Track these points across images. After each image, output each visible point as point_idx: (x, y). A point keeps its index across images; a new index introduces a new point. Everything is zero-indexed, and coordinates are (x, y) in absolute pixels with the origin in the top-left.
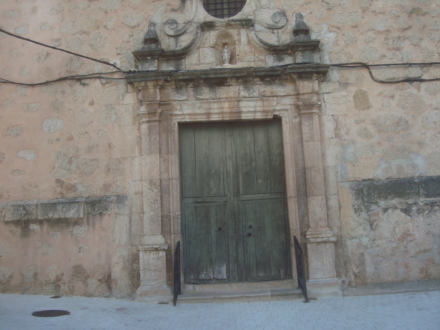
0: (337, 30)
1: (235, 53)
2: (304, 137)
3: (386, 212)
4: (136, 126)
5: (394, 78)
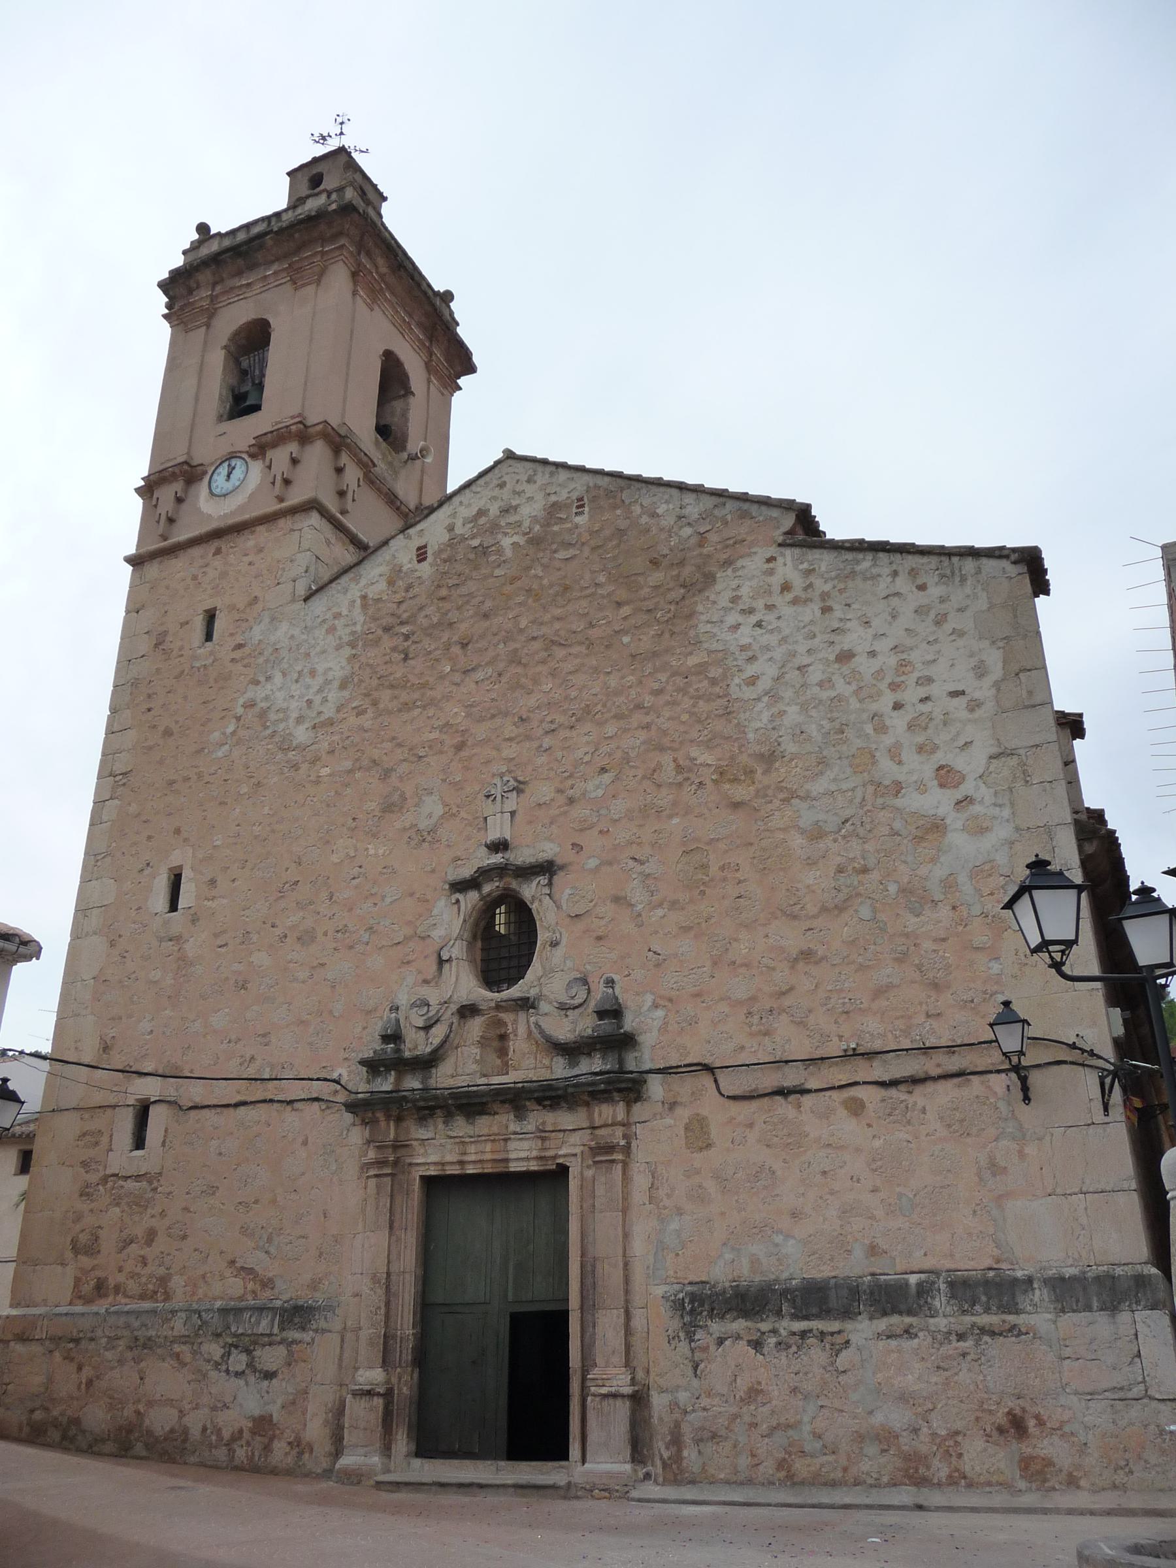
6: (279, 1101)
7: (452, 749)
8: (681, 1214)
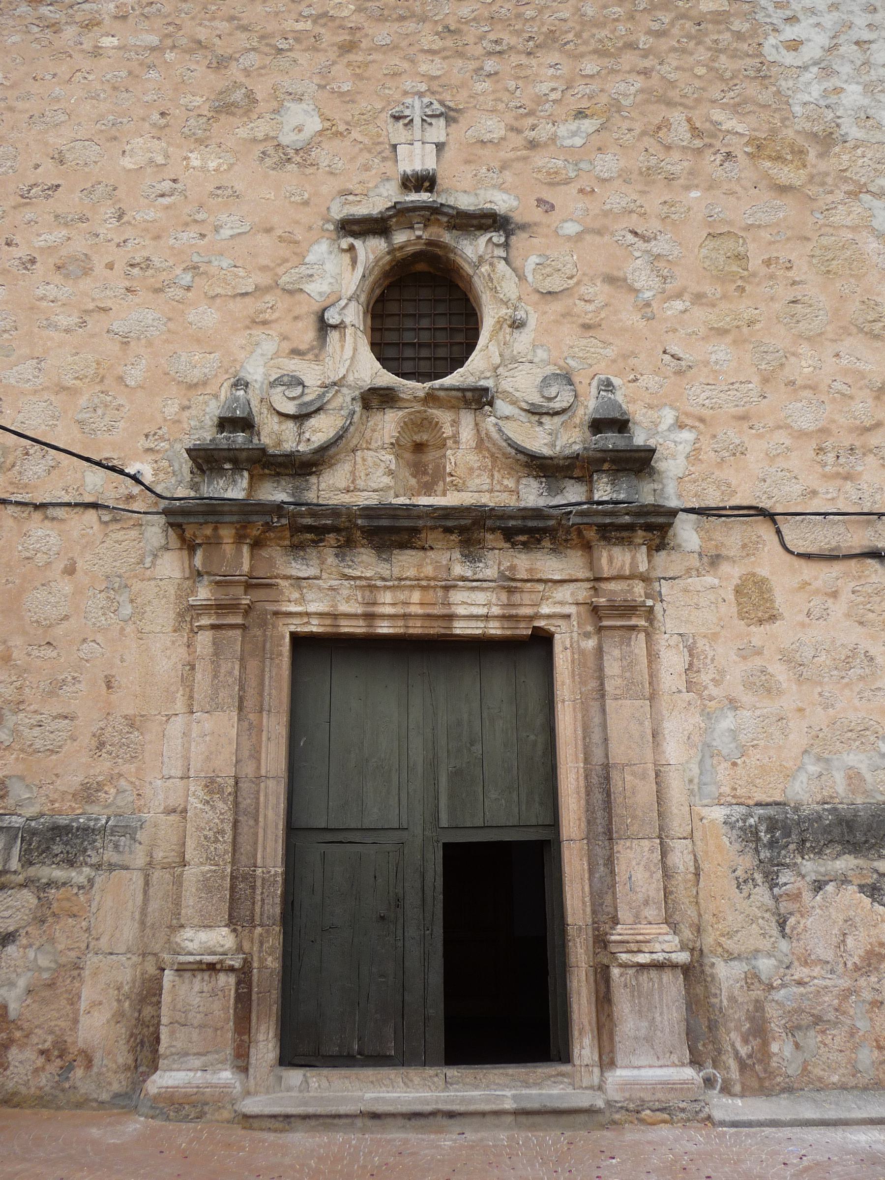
0: (697, 424)
1: (445, 467)
2: (609, 687)
3: (821, 892)
4: (183, 637)
5: (837, 548)
6: (18, 503)
7: (335, 48)
8: (736, 709)
